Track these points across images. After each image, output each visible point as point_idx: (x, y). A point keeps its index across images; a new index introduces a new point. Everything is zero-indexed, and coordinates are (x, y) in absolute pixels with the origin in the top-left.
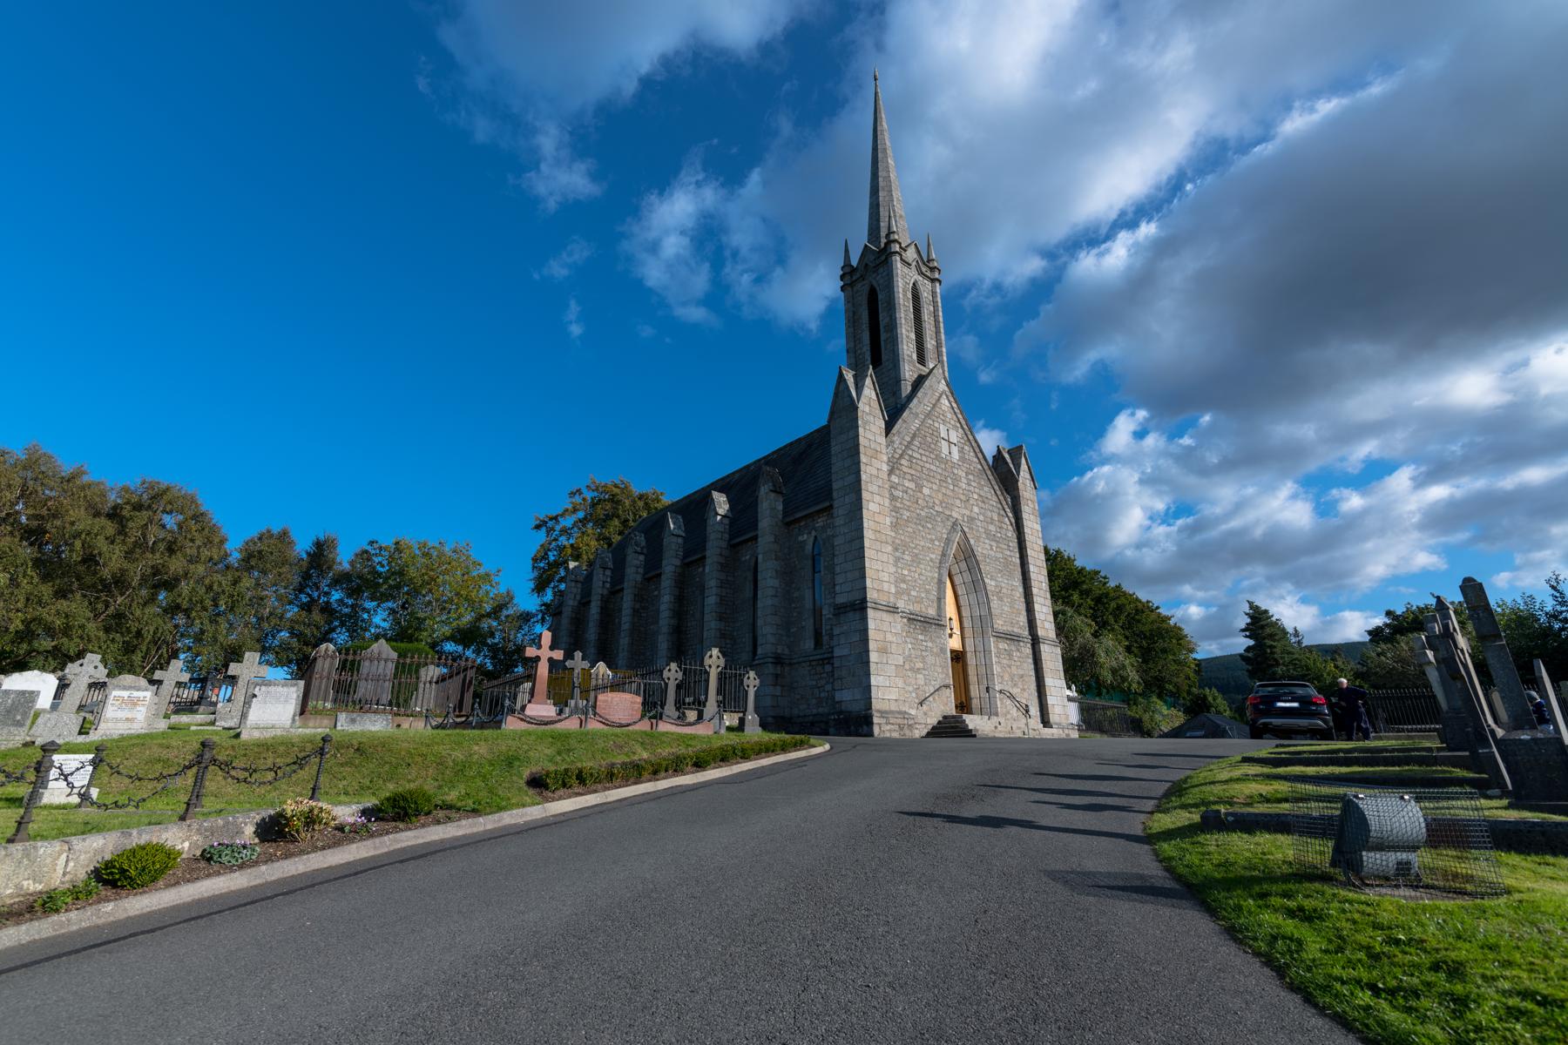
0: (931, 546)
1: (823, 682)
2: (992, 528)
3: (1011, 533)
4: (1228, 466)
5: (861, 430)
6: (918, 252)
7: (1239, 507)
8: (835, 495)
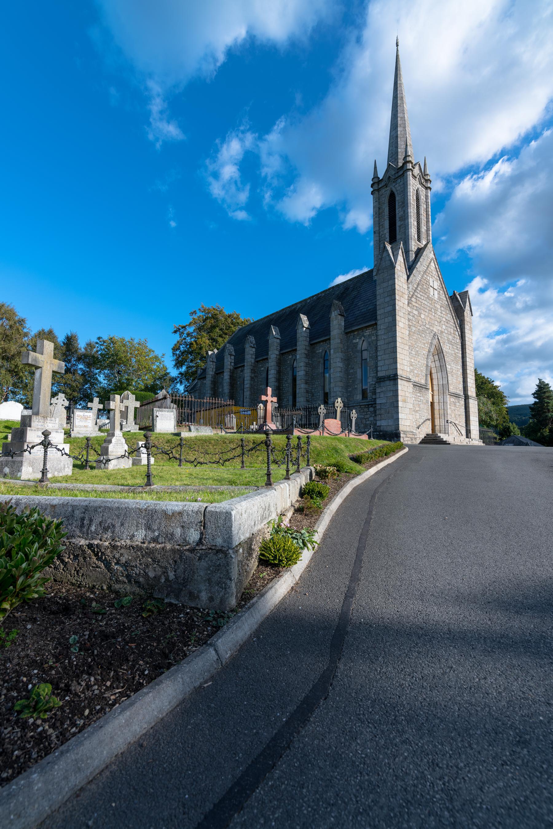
0: (424, 347)
1: (368, 416)
2: (450, 337)
3: (459, 341)
4: (527, 308)
5: (396, 280)
6: (420, 169)
7: (532, 329)
8: (378, 317)
